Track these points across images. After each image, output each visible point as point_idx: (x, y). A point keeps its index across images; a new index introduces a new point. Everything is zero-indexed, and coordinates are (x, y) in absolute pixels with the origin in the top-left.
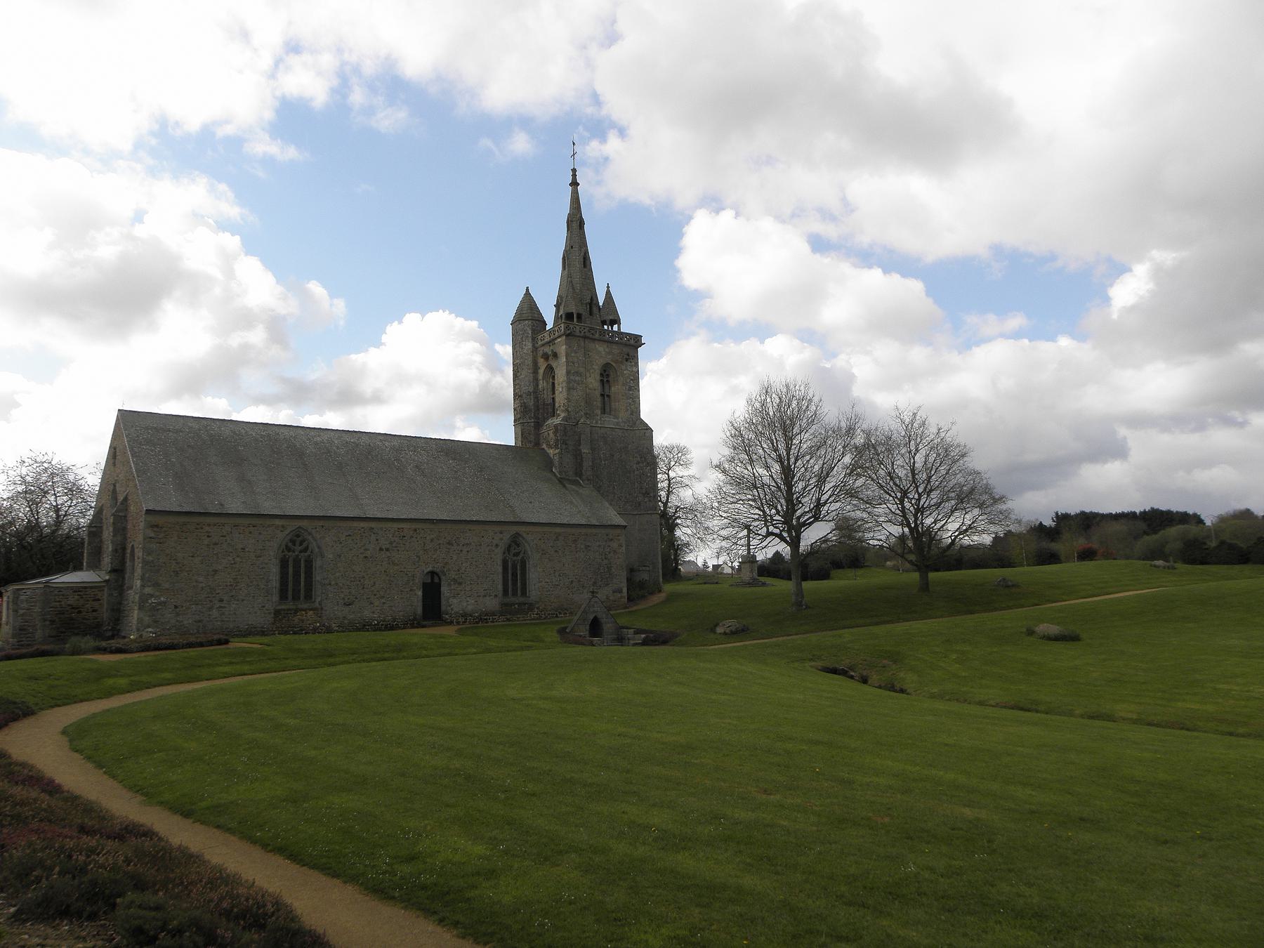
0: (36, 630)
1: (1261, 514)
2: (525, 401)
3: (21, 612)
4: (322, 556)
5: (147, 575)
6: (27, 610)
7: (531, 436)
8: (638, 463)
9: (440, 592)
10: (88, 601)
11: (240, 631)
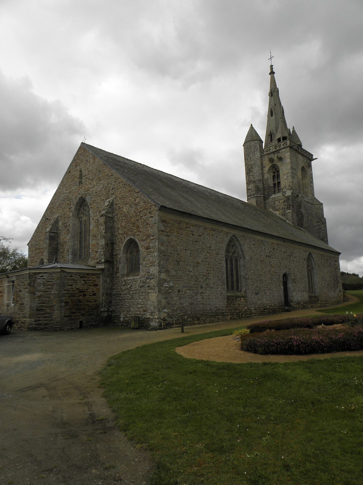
0: (53, 310)
1: (361, 276)
2: (257, 184)
3: (39, 294)
4: (244, 258)
5: (162, 263)
6: (44, 292)
7: (262, 204)
8: (317, 222)
9: (287, 287)
10: (90, 286)
11: (212, 312)
